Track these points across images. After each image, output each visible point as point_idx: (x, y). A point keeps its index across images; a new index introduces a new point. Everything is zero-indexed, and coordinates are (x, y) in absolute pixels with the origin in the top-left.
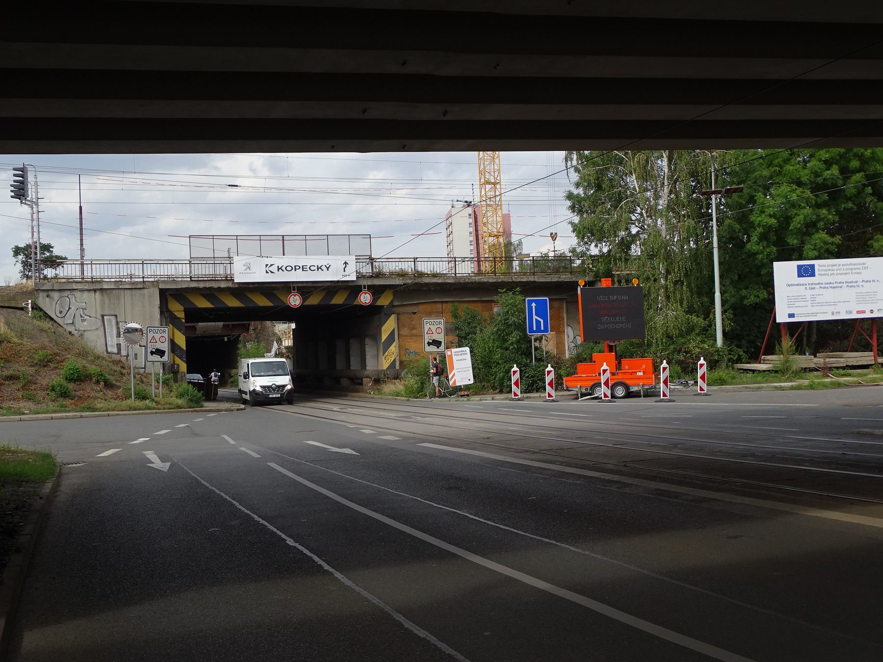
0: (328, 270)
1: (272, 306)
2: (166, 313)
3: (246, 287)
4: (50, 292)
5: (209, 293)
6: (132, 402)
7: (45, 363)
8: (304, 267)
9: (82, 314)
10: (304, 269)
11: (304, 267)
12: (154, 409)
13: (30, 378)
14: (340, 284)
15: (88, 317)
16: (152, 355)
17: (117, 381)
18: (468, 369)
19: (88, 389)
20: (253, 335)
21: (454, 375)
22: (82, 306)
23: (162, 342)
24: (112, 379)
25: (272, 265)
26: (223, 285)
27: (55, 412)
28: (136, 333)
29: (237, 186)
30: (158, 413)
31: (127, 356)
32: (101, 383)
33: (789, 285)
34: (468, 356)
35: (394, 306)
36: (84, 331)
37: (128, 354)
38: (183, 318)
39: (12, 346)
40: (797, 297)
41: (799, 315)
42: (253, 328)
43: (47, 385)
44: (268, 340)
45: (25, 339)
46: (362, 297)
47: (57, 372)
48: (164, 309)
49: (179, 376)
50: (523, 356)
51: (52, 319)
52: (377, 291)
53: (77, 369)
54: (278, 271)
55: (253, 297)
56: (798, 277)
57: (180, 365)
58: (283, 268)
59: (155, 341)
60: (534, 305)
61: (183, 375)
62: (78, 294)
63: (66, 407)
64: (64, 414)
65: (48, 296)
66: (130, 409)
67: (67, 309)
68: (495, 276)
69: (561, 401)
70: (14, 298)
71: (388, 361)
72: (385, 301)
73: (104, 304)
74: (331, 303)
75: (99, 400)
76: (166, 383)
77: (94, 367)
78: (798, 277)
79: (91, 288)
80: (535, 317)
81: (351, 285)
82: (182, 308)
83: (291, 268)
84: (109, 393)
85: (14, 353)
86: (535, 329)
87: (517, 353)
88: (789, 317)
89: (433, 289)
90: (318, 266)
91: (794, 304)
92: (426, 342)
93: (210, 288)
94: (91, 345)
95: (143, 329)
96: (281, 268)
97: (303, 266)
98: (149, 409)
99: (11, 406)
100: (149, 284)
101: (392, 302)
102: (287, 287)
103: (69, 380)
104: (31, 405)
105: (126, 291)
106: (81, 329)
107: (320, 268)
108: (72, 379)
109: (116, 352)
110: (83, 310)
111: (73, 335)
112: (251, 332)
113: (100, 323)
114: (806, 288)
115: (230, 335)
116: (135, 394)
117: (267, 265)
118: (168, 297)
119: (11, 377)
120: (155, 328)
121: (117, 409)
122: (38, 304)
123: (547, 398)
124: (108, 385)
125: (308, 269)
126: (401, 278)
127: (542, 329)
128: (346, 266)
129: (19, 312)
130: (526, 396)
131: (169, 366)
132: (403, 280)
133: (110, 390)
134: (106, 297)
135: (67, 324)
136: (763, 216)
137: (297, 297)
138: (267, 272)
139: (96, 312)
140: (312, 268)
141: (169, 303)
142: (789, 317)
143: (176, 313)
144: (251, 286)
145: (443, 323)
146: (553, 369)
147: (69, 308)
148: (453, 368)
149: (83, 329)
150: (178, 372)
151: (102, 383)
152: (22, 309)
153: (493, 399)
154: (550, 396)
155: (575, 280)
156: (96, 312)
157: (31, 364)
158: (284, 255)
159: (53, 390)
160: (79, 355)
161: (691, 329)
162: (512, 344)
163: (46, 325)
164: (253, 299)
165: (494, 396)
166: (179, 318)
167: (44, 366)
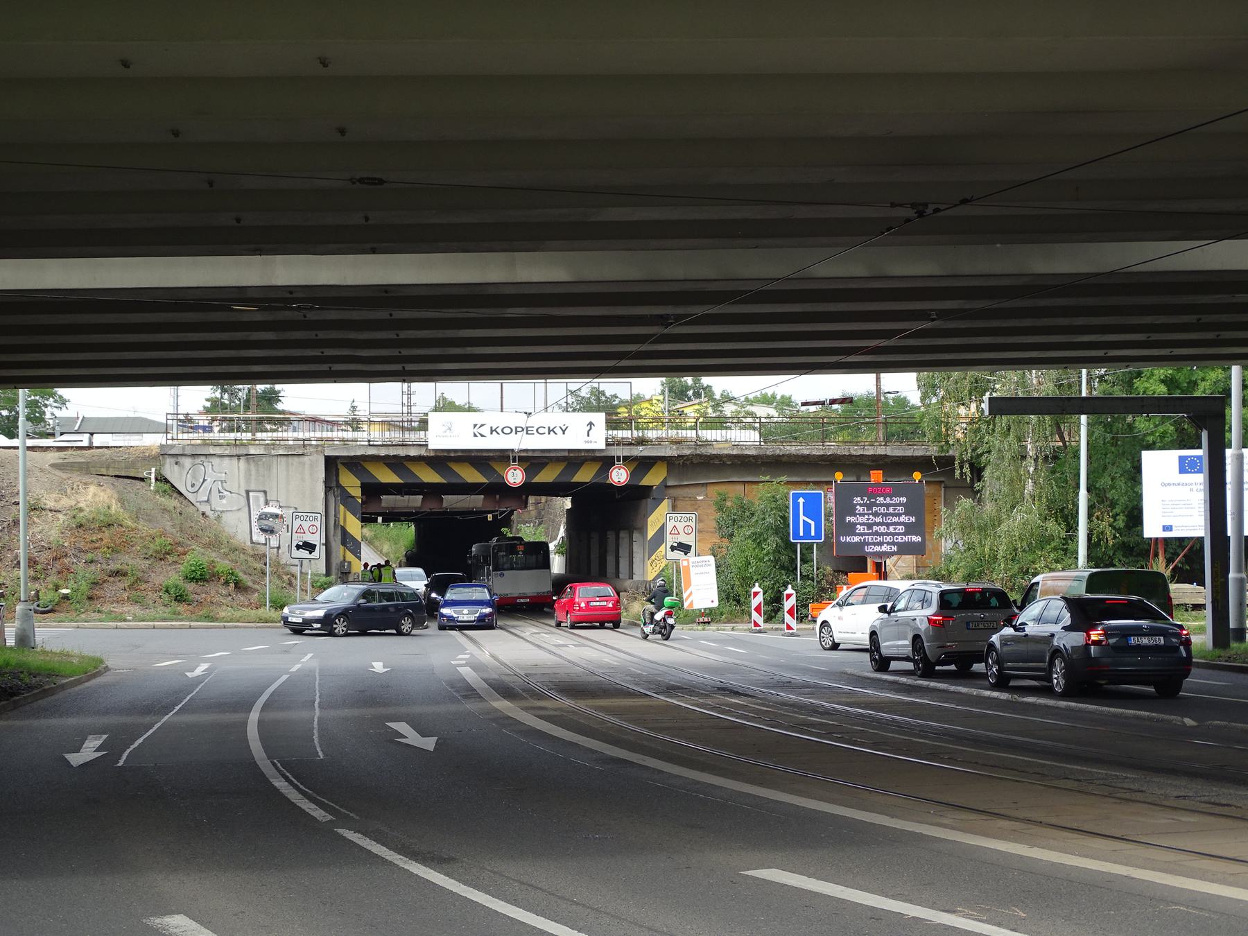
0: (564, 434)
3: (445, 456)
4: (179, 458)
5: (395, 463)
7: (162, 556)
8: (529, 429)
9: (220, 488)
10: (529, 432)
13: (141, 575)
14: (583, 454)
15: (229, 493)
17: (254, 582)
19: (215, 591)
20: (534, 513)
21: (691, 594)
22: (221, 477)
23: (313, 533)
24: (247, 580)
25: (482, 425)
26: (413, 452)
27: (164, 620)
31: (278, 548)
32: (231, 584)
33: (1166, 485)
36: (223, 512)
39: (124, 531)
40: (1177, 503)
41: (1180, 528)
42: (534, 502)
43: (161, 585)
44: (553, 521)
45: (142, 522)
47: (176, 569)
48: (334, 484)
51: (181, 494)
52: (644, 465)
53: (201, 564)
54: (492, 434)
56: (1180, 473)
58: (499, 430)
59: (676, 532)
60: (801, 500)
62: (216, 461)
63: (179, 614)
64: (169, 623)
65: (176, 463)
66: (260, 620)
67: (201, 481)
68: (823, 446)
69: (803, 636)
70: (133, 465)
71: (656, 569)
72: (653, 479)
73: (251, 475)
75: (224, 607)
77: (228, 562)
78: (1180, 473)
79: (235, 453)
80: (802, 518)
82: (359, 483)
83: (509, 430)
84: (241, 598)
85: (124, 540)
86: (801, 534)
87: (774, 567)
88: (1164, 530)
89: (729, 463)
90: (549, 428)
91: (1172, 512)
92: (669, 546)
93: (395, 457)
94: (229, 530)
95: (284, 516)
96: (495, 430)
97: (527, 428)
99: (112, 609)
102: (504, 457)
103: (190, 579)
104: (137, 609)
105: (279, 459)
106: (217, 509)
107: (553, 430)
108: (193, 578)
110: (222, 483)
111: (207, 517)
112: (530, 508)
113: (243, 501)
114: (1191, 490)
115: (497, 511)
117: (475, 426)
118: (341, 467)
119: (118, 572)
120: (302, 514)
121: (242, 620)
122: (164, 474)
124: (239, 587)
125: (535, 432)
126: (674, 447)
127: (813, 534)
128: (591, 429)
129: (138, 484)
130: (777, 627)
131: (337, 564)
132: (678, 449)
133: (243, 595)
134: (251, 461)
135: (200, 502)
136: (1151, 381)
138: (475, 435)
139: (239, 487)
140: (540, 431)
141: (340, 474)
142: (1164, 530)
143: (349, 490)
147: (204, 480)
149: (221, 509)
151: (232, 585)
152: (142, 479)
153: (733, 629)
154: (789, 627)
155: (953, 454)
156: (239, 487)
157: (144, 556)
159: (167, 591)
160: (209, 545)
161: (1044, 541)
162: (767, 554)
163: (172, 503)
164: (456, 471)
165: (735, 625)
166: (353, 497)
167: (161, 559)
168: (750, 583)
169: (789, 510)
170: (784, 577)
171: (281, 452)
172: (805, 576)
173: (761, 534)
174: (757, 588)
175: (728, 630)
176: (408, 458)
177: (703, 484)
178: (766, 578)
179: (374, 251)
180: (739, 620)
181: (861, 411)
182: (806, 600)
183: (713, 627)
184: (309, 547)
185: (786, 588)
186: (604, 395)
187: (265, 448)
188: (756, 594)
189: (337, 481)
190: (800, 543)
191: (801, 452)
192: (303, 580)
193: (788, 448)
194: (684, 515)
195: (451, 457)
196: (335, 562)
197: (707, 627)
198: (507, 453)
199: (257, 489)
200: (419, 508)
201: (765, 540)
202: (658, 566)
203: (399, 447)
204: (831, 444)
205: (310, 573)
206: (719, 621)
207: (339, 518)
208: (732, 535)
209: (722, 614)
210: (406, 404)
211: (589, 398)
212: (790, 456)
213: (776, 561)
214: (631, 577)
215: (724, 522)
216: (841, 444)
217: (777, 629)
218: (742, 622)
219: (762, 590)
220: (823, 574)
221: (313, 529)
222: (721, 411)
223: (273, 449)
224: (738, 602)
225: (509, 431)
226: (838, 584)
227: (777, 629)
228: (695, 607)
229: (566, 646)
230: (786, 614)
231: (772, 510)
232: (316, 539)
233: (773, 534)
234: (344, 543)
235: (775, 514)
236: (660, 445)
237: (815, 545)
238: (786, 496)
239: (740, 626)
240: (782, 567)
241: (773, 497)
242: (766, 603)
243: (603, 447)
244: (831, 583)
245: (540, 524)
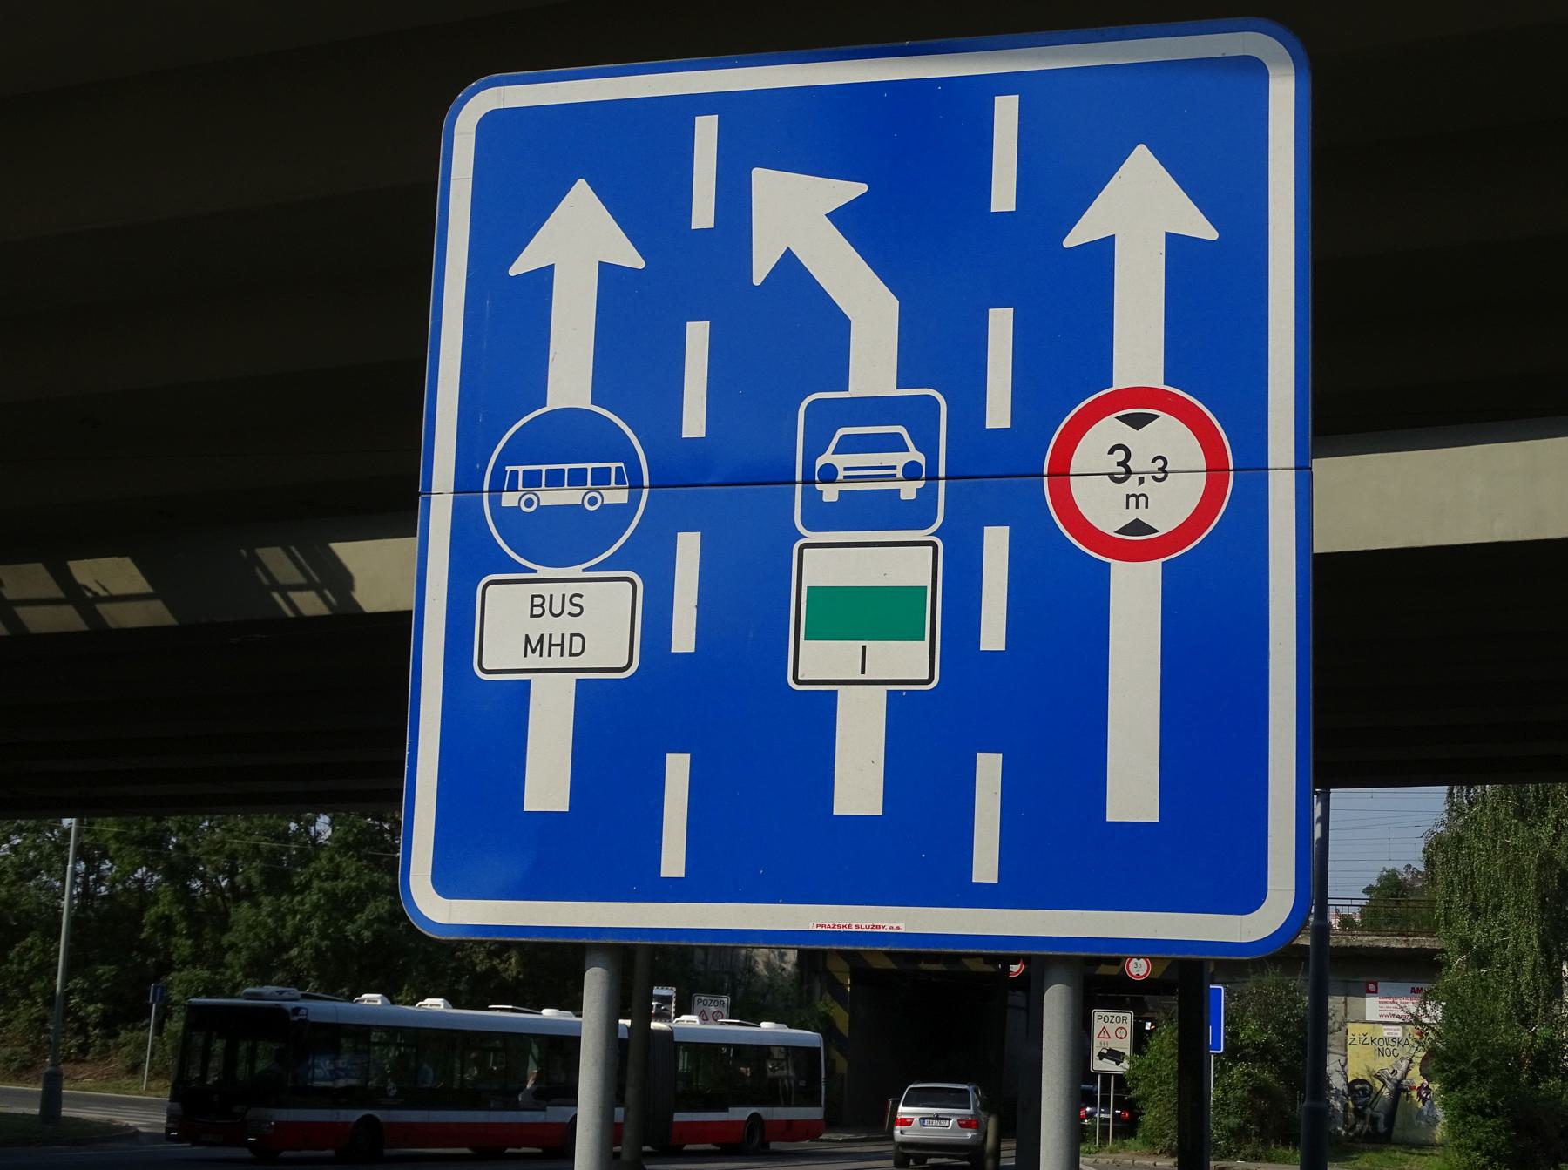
1: (992, 973)
8: (1142, 499)
10: (1132, 500)
11: (1142, 499)
16: (1101, 1059)
59: (1106, 1035)
74: (1097, 972)
82: (847, 967)
145: (1129, 1021)
191: (1377, 944)
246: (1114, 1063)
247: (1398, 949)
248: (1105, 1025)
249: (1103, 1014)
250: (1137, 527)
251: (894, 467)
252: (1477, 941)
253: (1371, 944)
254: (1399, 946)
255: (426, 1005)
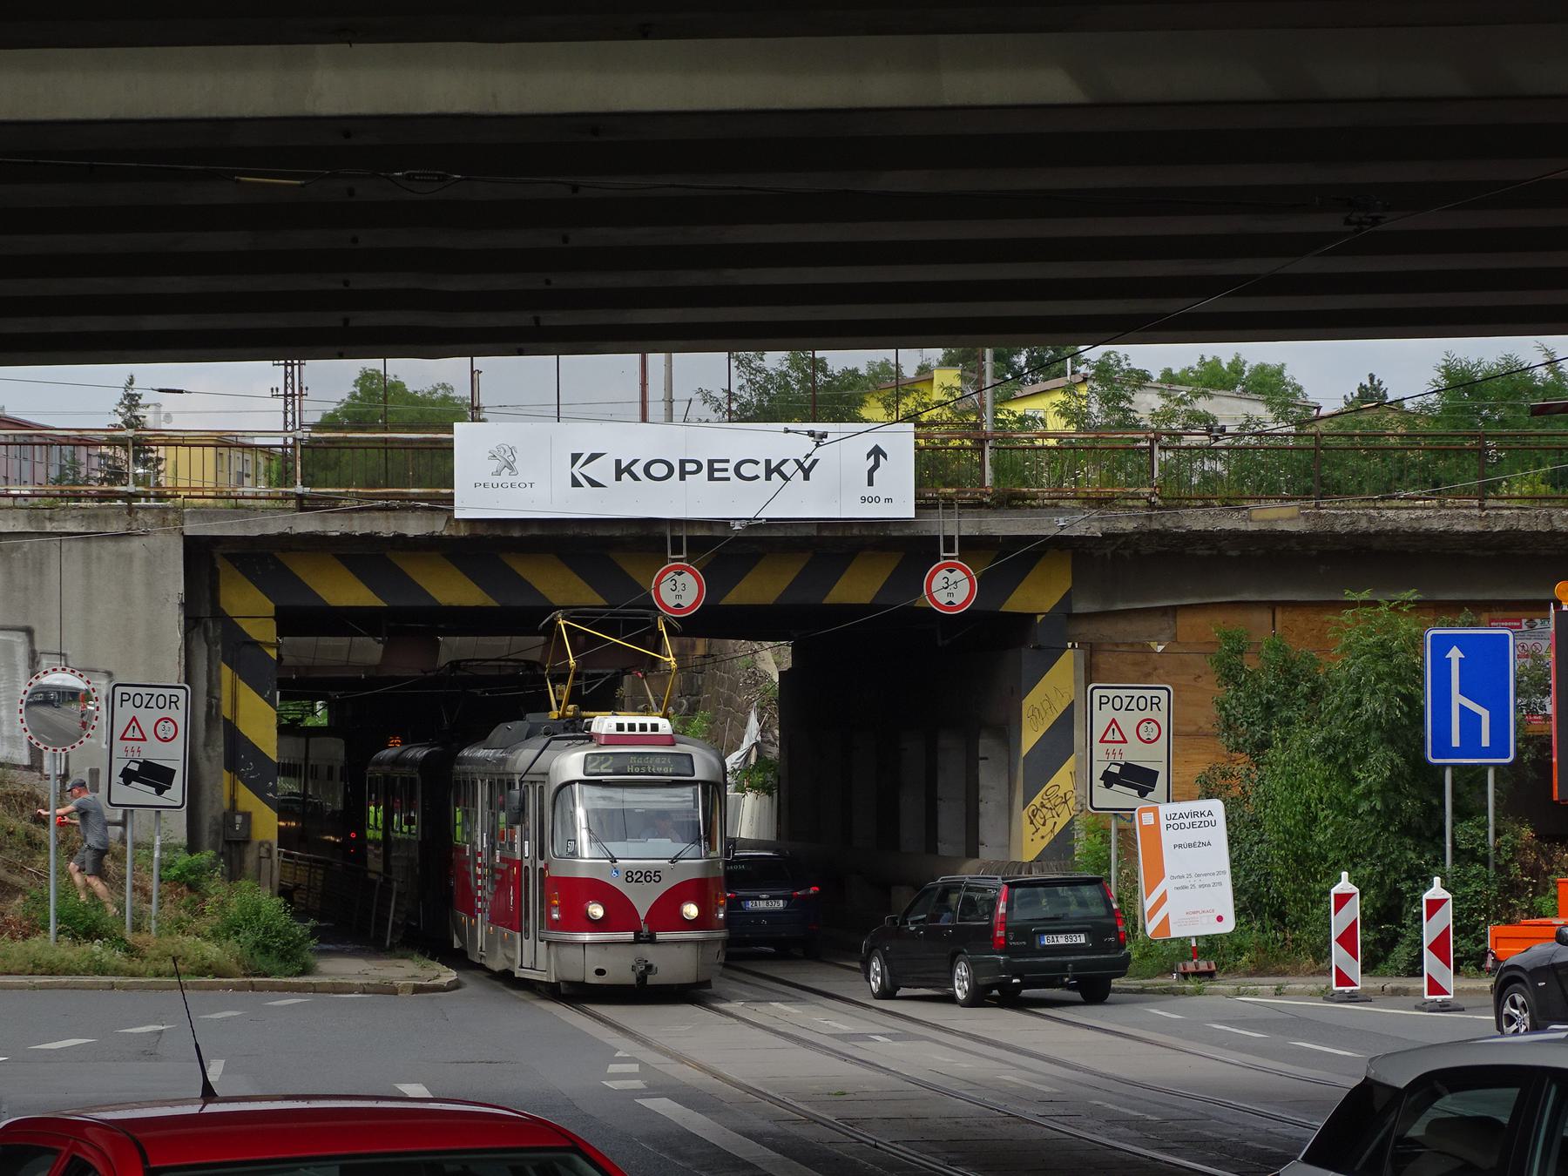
0: (806, 478)
2: (211, 624)
3: (499, 537)
6: (49, 945)
8: (716, 466)
10: (717, 475)
11: (716, 466)
12: (117, 971)
16: (127, 782)
18: (1216, 879)
21: (1163, 899)
25: (593, 457)
28: (74, 706)
29: (181, 392)
30: (120, 987)
34: (1219, 835)
35: (1073, 617)
37: (67, 770)
38: (270, 645)
44: (729, 702)
46: (938, 582)
48: (205, 610)
49: (250, 858)
50: (1408, 841)
54: (618, 478)
55: (528, 570)
57: (254, 816)
58: (638, 469)
59: (1118, 737)
60: (1455, 654)
61: (263, 852)
66: (37, 968)
68: (1482, 507)
71: (1044, 831)
74: (827, 601)
76: (188, 883)
80: (1457, 699)
81: (895, 534)
82: (270, 607)
86: (1456, 742)
87: (1385, 828)
89: (1234, 553)
90: (768, 462)
92: (1098, 774)
93: (370, 539)
96: (628, 470)
97: (711, 462)
98: (102, 970)
100: (149, 519)
101: (1067, 599)
107: (778, 469)
109: (26, 762)
116: (60, 918)
118: (223, 566)
123: (1335, 988)
125: (731, 473)
127: (1485, 742)
131: (215, 818)
137: (687, 578)
138: (576, 483)
140: (745, 470)
143: (246, 626)
144: (516, 533)
146: (1448, 895)
148: (1160, 875)
150: (247, 841)
153: (1279, 992)
154: (1435, 988)
158: (644, 419)
162: (1367, 794)
165: (1281, 980)
166: (256, 644)
168: (1316, 872)
169: (1423, 679)
170: (1411, 855)
171: (71, 527)
172: (1464, 852)
173: (1347, 743)
174: (1344, 885)
175: (1264, 995)
176: (400, 541)
177: (1164, 611)
178: (1361, 856)
179: (645, 33)
180: (1288, 968)
181: (1493, 409)
182: (1470, 916)
183: (1224, 985)
184: (156, 776)
185: (1429, 884)
186: (824, 370)
187: (29, 517)
188: (1342, 899)
189: (215, 600)
190: (1453, 766)
191: (1426, 525)
192: (141, 867)
193: (1390, 513)
194: (1137, 693)
195: (512, 538)
196: (210, 814)
197: (1209, 986)
198: (657, 530)
199: (9, 623)
200: (377, 667)
201: (1361, 758)
202: (1050, 823)
203: (377, 514)
204: (1501, 504)
205: (158, 843)
206: (1233, 971)
207: (219, 700)
208: (1264, 744)
209: (1239, 951)
210: (281, 392)
211: (784, 375)
212: (1395, 534)
213: (1390, 813)
214: (972, 850)
215: (1241, 709)
216: (1526, 504)
217: (1395, 992)
218: (1297, 972)
219: (1356, 890)
220: (1514, 849)
221: (166, 730)
222: (1126, 411)
223: (51, 519)
224: (1280, 915)
225: (654, 470)
226: (1551, 872)
227: (1395, 992)
228: (1175, 932)
229: (864, 1037)
230: (1428, 956)
231: (1380, 679)
232: (172, 755)
233: (1382, 741)
234: (232, 764)
235: (1386, 691)
236: (1056, 506)
237: (1491, 773)
238: (1416, 643)
239: (1297, 984)
240: (1406, 830)
241: (1382, 645)
242: (1370, 920)
243: (906, 509)
244: (1534, 871)
245: (693, 709)
246: (153, 790)
247: (1468, 534)
248: (1117, 715)
249: (1111, 693)
250: (679, 605)
251: (727, 461)
252: (1551, 516)
253: (1416, 525)
254: (1468, 529)
255: (574, 805)
